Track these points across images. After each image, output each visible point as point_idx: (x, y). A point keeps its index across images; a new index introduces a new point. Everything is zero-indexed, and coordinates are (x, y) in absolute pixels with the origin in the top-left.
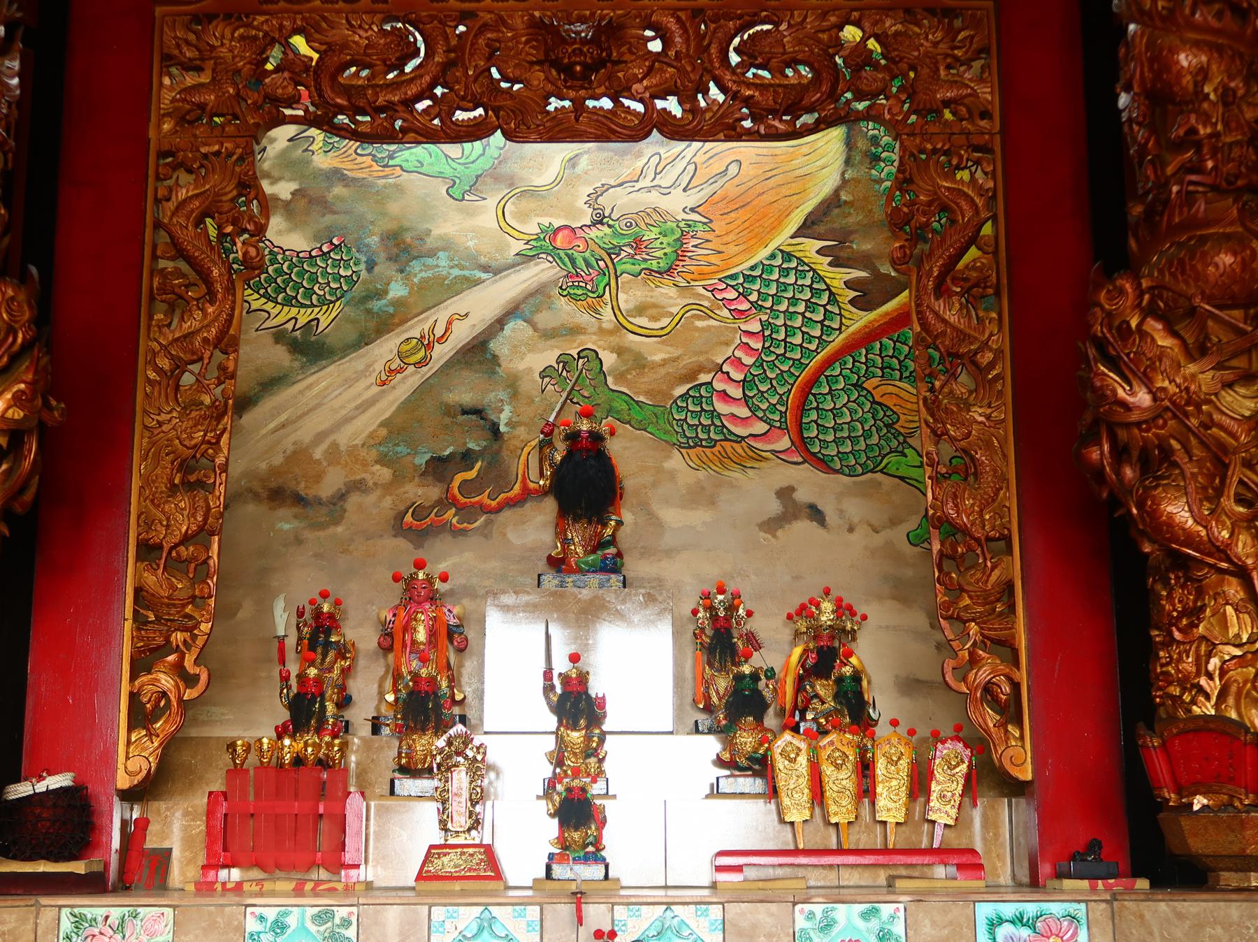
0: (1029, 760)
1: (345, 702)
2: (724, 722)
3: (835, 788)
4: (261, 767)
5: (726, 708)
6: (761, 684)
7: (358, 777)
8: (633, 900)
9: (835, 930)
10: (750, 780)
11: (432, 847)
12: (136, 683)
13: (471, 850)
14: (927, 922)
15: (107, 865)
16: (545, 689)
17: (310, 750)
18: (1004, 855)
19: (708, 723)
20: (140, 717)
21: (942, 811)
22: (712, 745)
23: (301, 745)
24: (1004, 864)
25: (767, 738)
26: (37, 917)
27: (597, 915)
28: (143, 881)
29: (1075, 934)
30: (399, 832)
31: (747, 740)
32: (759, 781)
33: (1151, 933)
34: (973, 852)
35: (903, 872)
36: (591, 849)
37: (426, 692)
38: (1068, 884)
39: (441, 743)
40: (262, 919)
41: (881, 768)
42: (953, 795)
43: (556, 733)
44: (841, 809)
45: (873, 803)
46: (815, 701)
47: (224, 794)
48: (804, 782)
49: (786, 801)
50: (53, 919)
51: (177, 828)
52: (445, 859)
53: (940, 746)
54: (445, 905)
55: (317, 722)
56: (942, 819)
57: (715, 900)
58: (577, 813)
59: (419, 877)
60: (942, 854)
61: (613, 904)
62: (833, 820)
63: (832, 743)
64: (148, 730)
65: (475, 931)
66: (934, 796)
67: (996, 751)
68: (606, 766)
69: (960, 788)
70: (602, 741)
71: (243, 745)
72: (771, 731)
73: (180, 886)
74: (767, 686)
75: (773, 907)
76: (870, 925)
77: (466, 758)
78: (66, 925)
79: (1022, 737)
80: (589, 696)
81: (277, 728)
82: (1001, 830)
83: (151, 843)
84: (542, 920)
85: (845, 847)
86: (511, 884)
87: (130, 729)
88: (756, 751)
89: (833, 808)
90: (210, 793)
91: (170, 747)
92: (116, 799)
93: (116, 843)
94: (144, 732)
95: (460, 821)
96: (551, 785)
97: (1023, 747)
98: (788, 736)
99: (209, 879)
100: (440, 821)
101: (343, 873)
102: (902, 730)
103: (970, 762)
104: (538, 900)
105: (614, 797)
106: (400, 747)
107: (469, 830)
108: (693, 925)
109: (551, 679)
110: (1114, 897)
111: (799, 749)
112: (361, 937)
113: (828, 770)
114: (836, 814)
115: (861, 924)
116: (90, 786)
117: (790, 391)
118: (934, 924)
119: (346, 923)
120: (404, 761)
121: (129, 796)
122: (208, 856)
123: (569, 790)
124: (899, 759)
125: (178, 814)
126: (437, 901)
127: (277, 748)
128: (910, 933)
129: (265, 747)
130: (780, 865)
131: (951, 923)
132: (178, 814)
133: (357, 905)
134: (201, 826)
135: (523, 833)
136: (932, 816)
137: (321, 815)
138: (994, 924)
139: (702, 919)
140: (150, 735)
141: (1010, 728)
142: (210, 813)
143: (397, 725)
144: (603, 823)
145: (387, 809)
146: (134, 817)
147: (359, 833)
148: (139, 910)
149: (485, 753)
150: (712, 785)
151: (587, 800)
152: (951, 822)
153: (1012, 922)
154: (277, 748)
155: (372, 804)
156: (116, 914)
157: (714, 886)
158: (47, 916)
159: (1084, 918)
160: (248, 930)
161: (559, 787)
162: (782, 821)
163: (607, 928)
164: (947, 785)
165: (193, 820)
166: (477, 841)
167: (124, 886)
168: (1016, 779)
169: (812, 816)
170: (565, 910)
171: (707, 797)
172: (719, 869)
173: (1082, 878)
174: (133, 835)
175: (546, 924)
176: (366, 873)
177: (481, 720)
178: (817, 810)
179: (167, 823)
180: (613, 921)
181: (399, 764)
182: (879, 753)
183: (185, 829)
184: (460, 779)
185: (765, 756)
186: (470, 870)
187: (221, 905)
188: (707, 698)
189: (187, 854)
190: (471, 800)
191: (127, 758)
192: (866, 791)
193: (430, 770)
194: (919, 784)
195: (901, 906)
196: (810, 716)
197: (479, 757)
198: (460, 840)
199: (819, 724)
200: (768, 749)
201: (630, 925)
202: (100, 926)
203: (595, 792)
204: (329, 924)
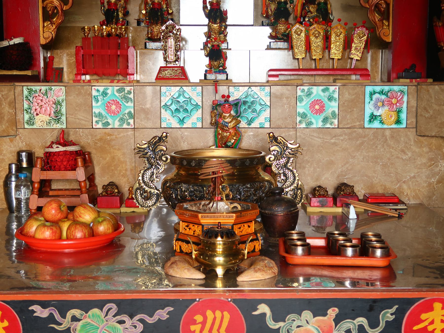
0: (391, 34)
1: (126, 14)
2: (273, 21)
3: (315, 46)
4: (95, 37)
5: (274, 15)
6: (288, 6)
7: (132, 42)
8: (237, 85)
9: (312, 96)
10: (282, 43)
11: (161, 67)
12: (45, 3)
13: (176, 69)
14: (347, 93)
15: (39, 73)
16: (203, 7)
17: (113, 30)
18: (379, 71)
19: (267, 22)
20: (47, 17)
21: (356, 55)
22: (268, 30)
23: (110, 28)
24: (378, 74)
25: (289, 26)
26: (14, 90)
27: (223, 90)
28: (54, 80)
29: (402, 98)
30: (149, 62)
31: (282, 28)
32: (286, 44)
33: (431, 97)
34: (367, 70)
35: (340, 78)
36: (221, 68)
37: (158, 8)
38: (401, 80)
39: (164, 28)
40: (98, 91)
41: (333, 39)
42: (361, 48)
43: (208, 25)
44: (317, 54)
45: (329, 51)
46: (309, 13)
47: (82, 47)
48: (303, 43)
49: (296, 51)
50: (21, 91)
51: (65, 60)
52: (166, 72)
53: (356, 29)
54: (166, 86)
55: (115, 20)
56: (356, 58)
57: (267, 85)
58: (216, 55)
59: (157, 79)
60: (355, 71)
61: (229, 86)
62: (314, 58)
63: (314, 28)
64: (51, 21)
65: (177, 96)
66: (353, 49)
67: (378, 31)
68: (228, 38)
69: (363, 45)
70: (226, 28)
71: (87, 28)
72: (291, 24)
73: (67, 81)
74: (290, 6)
75: (289, 87)
76: (325, 94)
77: (173, 33)
78: (26, 92)
79: (389, 25)
80: (221, 10)
81: (100, 22)
82: (379, 61)
83: (55, 66)
84: (202, 92)
85: (318, 68)
86: (191, 81)
87: (44, 21)
88: (285, 32)
89: (314, 53)
90: (76, 47)
91: (59, 29)
92: (40, 48)
93: (42, 65)
94: (49, 23)
95: (172, 57)
96: (206, 44)
97: (389, 29)
98: (297, 25)
99: (78, 79)
100: (164, 58)
101: (128, 77)
102: (342, 22)
103: (368, 35)
104: (201, 84)
105: (230, 49)
106: (148, 30)
107: (175, 61)
108: (259, 94)
109: (206, 3)
110: (418, 84)
111: (302, 31)
112: (135, 98)
113: (312, 38)
114: (315, 55)
115: (322, 94)
116: (30, 43)
118: (349, 94)
119: (129, 92)
120: (150, 35)
121: (46, 47)
122: (77, 71)
123: (213, 46)
124: (340, 34)
125: (65, 55)
126: (163, 85)
127: (100, 30)
128: (340, 97)
129: (96, 29)
130: (293, 75)
131: (356, 93)
132: (65, 55)
133: (133, 86)
134: (74, 59)
135: (196, 62)
136: (352, 56)
137: (119, 55)
138: (372, 94)
139: (262, 92)
140: (52, 23)
141: (384, 21)
142: (77, 54)
143: (146, 22)
144: (226, 58)
145: (144, 53)
146: (48, 56)
147: (133, 62)
148: (52, 87)
149: (180, 32)
150: (268, 46)
151: (220, 50)
152: (359, 59)
153: (379, 93)
154: (100, 30)
155: (138, 51)
156: (44, 88)
157: (268, 82)
158: (18, 89)
159: (406, 92)
160: (93, 95)
161: (209, 45)
162: (294, 58)
163: (226, 94)
164: (358, 44)
165: (71, 57)
166: (178, 65)
167: (46, 80)
168: (385, 41)
169: (306, 56)
170: (211, 88)
171: (266, 49)
172: (270, 76)
173: (407, 78)
174: (49, 63)
175: (204, 93)
176: (136, 77)
177: (179, 21)
178: (308, 54)
179: (61, 58)
180: (229, 92)
181: (148, 36)
182: (333, 32)
183: (68, 60)
184: (171, 42)
185: (289, 34)
186: (176, 76)
187: (83, 86)
188: (267, 12)
189: (69, 70)
190: (175, 50)
191: (44, 32)
192: (327, 46)
193: (160, 38)
194: (347, 45)
195: (337, 87)
196: (307, 19)
197: (178, 33)
198: (172, 65)
199: (310, 22)
200: (290, 30)
201: (235, 94)
202: (38, 93)
203: (223, 48)
204: (123, 93)
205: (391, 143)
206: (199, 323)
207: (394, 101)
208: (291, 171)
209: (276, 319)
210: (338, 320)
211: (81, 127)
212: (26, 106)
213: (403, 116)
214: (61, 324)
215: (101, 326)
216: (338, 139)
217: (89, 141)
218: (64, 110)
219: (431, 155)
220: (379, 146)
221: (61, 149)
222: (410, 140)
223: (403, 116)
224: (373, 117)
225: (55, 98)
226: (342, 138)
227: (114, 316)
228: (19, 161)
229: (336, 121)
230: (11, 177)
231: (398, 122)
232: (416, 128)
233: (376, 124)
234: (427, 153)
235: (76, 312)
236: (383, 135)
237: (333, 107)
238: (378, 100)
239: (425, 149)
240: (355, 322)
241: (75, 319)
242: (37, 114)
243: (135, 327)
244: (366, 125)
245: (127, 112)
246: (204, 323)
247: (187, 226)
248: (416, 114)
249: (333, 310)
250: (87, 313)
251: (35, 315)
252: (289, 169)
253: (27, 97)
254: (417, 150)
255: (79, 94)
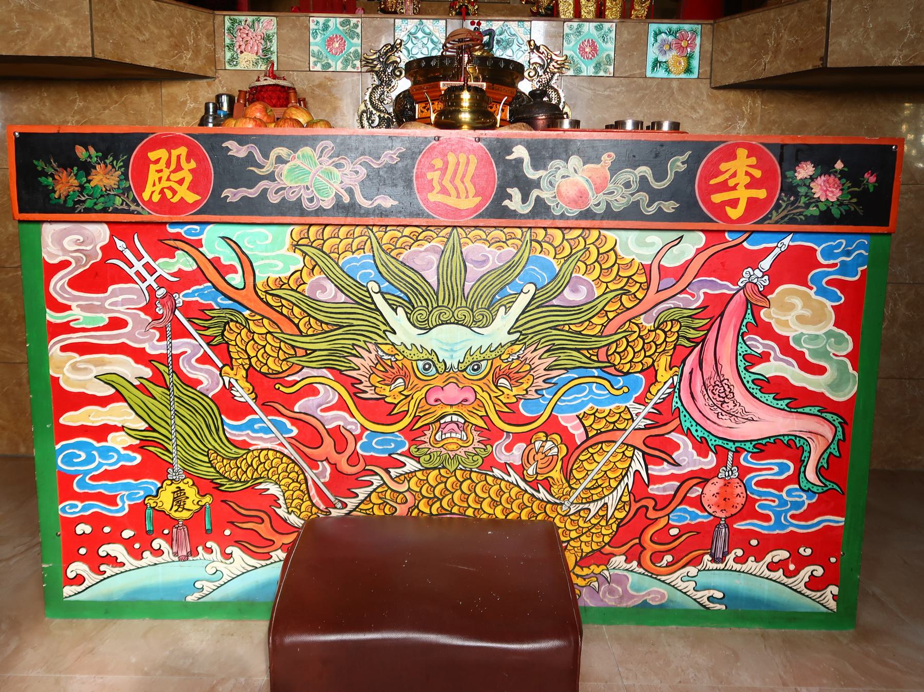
14: (843, 45)
29: (695, 39)
78: (228, 24)
88: (549, 5)
117: (292, 290)
156: (250, 19)
158: (219, 19)
205: (679, 97)
206: (438, 169)
207: (683, 44)
208: (556, 90)
209: (535, 167)
210: (614, 169)
211: (295, 69)
212: (228, 41)
213: (695, 63)
214: (262, 167)
215: (313, 171)
216: (613, 91)
217: (305, 87)
218: (274, 48)
219: (728, 114)
220: (664, 102)
221: (271, 81)
222: (702, 94)
223: (695, 63)
224: (657, 63)
225: (264, 31)
226: (618, 90)
227: (330, 157)
228: (218, 105)
229: (611, 68)
230: (208, 118)
231: (688, 70)
232: (711, 78)
233: (661, 73)
234: (723, 111)
235: (282, 151)
236: (670, 87)
237: (608, 48)
238: (664, 41)
239: (721, 107)
240: (636, 172)
241: (280, 160)
242: (242, 52)
243: (357, 172)
244: (649, 74)
245: (352, 50)
246: (444, 170)
247: (424, 108)
248: (710, 60)
249: (609, 156)
250: (295, 152)
251: (230, 153)
252: (552, 88)
253: (229, 30)
254: (711, 107)
255: (294, 27)
